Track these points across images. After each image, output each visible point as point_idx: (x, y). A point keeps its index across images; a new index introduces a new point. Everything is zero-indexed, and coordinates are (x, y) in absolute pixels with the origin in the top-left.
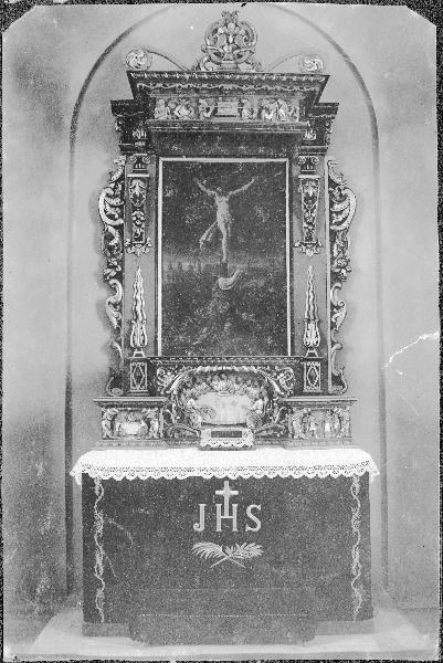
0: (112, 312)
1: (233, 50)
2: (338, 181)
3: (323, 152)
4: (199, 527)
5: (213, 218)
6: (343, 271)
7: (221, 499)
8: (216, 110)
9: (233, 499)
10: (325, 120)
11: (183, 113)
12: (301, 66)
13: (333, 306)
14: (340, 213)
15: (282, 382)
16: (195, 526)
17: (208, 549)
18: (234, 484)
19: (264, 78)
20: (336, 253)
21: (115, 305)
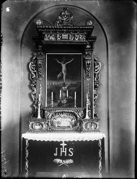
4: (56, 155)
7: (62, 147)
8: (62, 38)
9: (65, 147)
11: (52, 38)
15: (80, 115)
17: (58, 161)
18: (65, 142)
21: (34, 94)
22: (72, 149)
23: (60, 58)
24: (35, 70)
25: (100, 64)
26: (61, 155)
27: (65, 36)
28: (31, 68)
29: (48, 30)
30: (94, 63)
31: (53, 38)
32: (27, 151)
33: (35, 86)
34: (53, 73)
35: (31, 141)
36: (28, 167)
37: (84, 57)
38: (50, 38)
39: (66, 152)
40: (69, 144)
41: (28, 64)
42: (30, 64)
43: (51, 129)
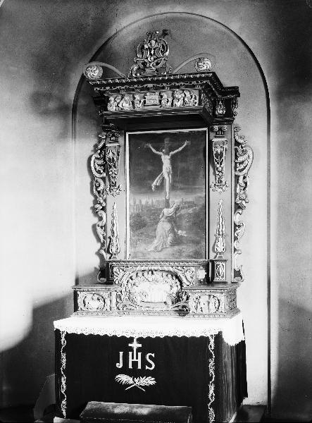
0: (100, 231)
1: (154, 59)
2: (240, 141)
3: (230, 122)
4: (120, 365)
5: (161, 170)
6: (244, 202)
7: (131, 349)
8: (145, 102)
9: (138, 350)
10: (230, 99)
11: (126, 106)
12: (196, 67)
13: (235, 225)
14: (242, 163)
15: (188, 277)
16: (117, 364)
17: (124, 378)
18: (140, 340)
19: (172, 78)
20: (238, 191)
21: (102, 227)
22: (153, 355)
23: (157, 140)
24: (104, 171)
25: (250, 152)
26: (130, 367)
27: (152, 98)
28: (95, 169)
29: (116, 88)
30: (236, 150)
31: (127, 105)
32: (64, 356)
33: (104, 209)
34: (144, 176)
35: (71, 337)
36: (67, 387)
37: (211, 138)
38: (120, 104)
39: (139, 361)
40: (148, 344)
41: (90, 159)
42: (93, 158)
43: (126, 306)
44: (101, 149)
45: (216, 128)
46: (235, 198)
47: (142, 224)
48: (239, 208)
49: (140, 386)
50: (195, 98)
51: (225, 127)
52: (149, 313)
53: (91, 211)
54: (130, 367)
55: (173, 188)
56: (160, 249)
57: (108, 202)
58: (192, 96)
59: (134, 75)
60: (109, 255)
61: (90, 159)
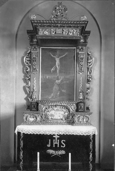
0: (27, 89)
4: (49, 146)
6: (90, 79)
7: (55, 138)
8: (56, 32)
9: (58, 139)
11: (46, 33)
15: (73, 108)
17: (51, 151)
21: (28, 87)
24: (30, 63)
25: (93, 59)
26: (54, 146)
27: (59, 31)
28: (26, 62)
32: (22, 142)
33: (29, 79)
34: (47, 67)
37: (77, 52)
40: (62, 137)
41: (23, 58)
43: (45, 120)
44: (29, 53)
45: (80, 47)
46: (87, 77)
47: (46, 86)
48: (89, 81)
49: (58, 155)
50: (78, 32)
51: (84, 48)
52: (57, 123)
53: (23, 81)
54: (54, 146)
55: (60, 72)
56: (54, 97)
57: (31, 76)
58: (77, 31)
59: (52, 20)
60: (31, 100)
61: (23, 58)
